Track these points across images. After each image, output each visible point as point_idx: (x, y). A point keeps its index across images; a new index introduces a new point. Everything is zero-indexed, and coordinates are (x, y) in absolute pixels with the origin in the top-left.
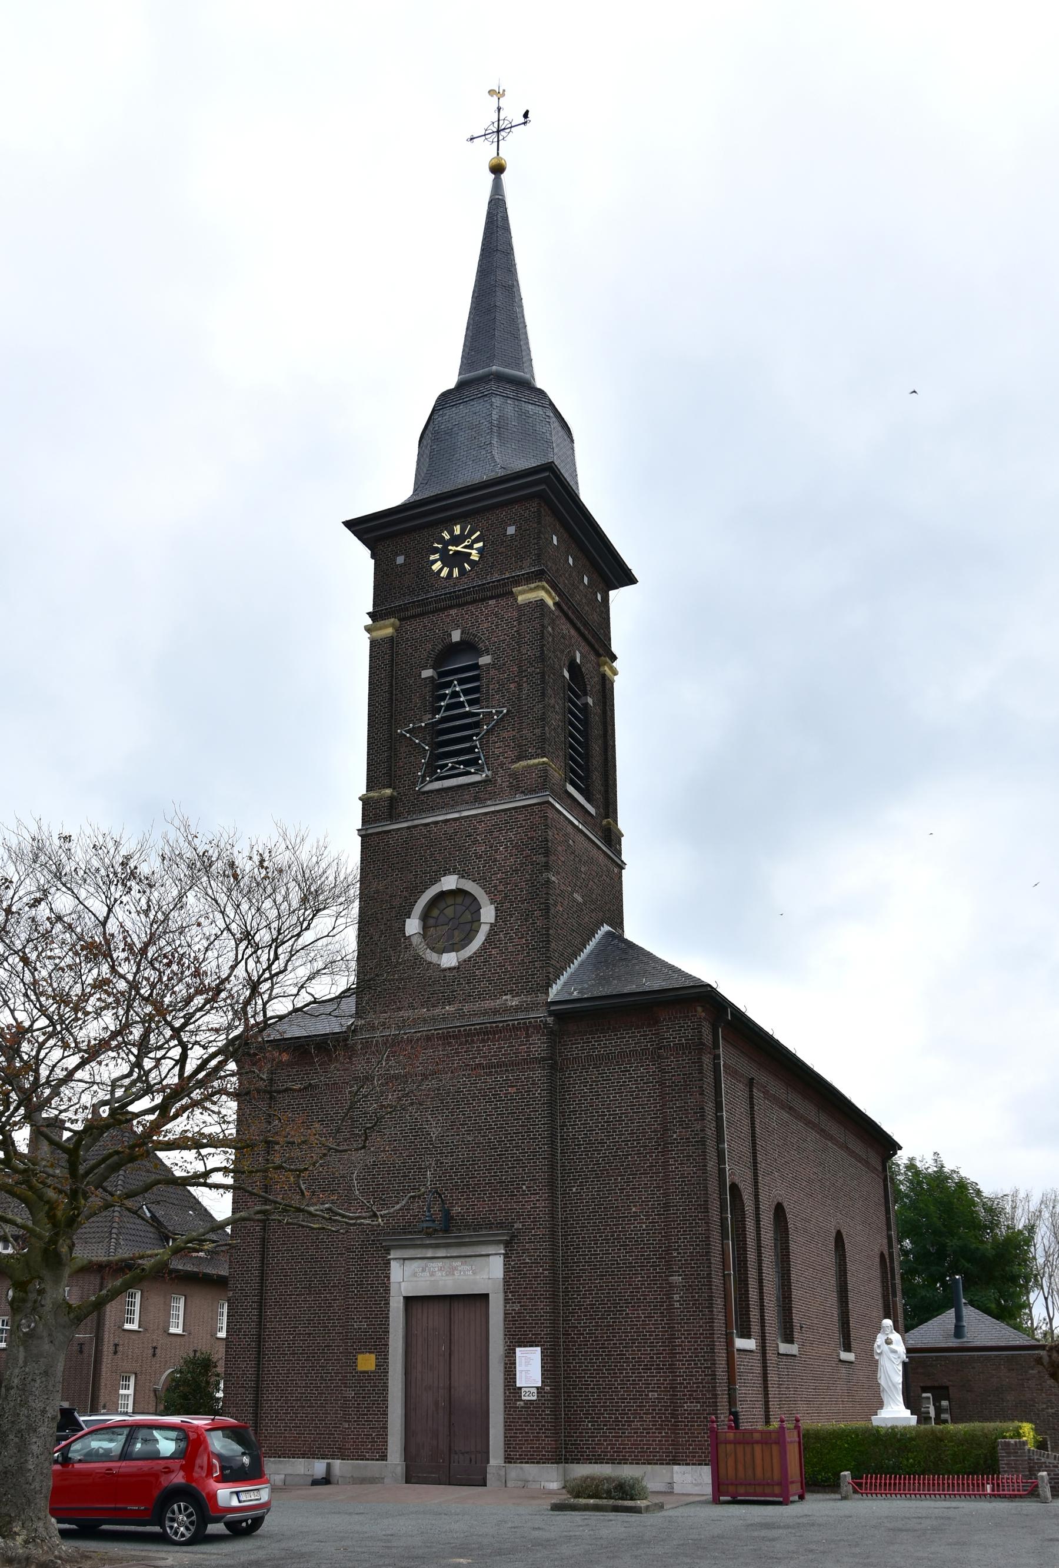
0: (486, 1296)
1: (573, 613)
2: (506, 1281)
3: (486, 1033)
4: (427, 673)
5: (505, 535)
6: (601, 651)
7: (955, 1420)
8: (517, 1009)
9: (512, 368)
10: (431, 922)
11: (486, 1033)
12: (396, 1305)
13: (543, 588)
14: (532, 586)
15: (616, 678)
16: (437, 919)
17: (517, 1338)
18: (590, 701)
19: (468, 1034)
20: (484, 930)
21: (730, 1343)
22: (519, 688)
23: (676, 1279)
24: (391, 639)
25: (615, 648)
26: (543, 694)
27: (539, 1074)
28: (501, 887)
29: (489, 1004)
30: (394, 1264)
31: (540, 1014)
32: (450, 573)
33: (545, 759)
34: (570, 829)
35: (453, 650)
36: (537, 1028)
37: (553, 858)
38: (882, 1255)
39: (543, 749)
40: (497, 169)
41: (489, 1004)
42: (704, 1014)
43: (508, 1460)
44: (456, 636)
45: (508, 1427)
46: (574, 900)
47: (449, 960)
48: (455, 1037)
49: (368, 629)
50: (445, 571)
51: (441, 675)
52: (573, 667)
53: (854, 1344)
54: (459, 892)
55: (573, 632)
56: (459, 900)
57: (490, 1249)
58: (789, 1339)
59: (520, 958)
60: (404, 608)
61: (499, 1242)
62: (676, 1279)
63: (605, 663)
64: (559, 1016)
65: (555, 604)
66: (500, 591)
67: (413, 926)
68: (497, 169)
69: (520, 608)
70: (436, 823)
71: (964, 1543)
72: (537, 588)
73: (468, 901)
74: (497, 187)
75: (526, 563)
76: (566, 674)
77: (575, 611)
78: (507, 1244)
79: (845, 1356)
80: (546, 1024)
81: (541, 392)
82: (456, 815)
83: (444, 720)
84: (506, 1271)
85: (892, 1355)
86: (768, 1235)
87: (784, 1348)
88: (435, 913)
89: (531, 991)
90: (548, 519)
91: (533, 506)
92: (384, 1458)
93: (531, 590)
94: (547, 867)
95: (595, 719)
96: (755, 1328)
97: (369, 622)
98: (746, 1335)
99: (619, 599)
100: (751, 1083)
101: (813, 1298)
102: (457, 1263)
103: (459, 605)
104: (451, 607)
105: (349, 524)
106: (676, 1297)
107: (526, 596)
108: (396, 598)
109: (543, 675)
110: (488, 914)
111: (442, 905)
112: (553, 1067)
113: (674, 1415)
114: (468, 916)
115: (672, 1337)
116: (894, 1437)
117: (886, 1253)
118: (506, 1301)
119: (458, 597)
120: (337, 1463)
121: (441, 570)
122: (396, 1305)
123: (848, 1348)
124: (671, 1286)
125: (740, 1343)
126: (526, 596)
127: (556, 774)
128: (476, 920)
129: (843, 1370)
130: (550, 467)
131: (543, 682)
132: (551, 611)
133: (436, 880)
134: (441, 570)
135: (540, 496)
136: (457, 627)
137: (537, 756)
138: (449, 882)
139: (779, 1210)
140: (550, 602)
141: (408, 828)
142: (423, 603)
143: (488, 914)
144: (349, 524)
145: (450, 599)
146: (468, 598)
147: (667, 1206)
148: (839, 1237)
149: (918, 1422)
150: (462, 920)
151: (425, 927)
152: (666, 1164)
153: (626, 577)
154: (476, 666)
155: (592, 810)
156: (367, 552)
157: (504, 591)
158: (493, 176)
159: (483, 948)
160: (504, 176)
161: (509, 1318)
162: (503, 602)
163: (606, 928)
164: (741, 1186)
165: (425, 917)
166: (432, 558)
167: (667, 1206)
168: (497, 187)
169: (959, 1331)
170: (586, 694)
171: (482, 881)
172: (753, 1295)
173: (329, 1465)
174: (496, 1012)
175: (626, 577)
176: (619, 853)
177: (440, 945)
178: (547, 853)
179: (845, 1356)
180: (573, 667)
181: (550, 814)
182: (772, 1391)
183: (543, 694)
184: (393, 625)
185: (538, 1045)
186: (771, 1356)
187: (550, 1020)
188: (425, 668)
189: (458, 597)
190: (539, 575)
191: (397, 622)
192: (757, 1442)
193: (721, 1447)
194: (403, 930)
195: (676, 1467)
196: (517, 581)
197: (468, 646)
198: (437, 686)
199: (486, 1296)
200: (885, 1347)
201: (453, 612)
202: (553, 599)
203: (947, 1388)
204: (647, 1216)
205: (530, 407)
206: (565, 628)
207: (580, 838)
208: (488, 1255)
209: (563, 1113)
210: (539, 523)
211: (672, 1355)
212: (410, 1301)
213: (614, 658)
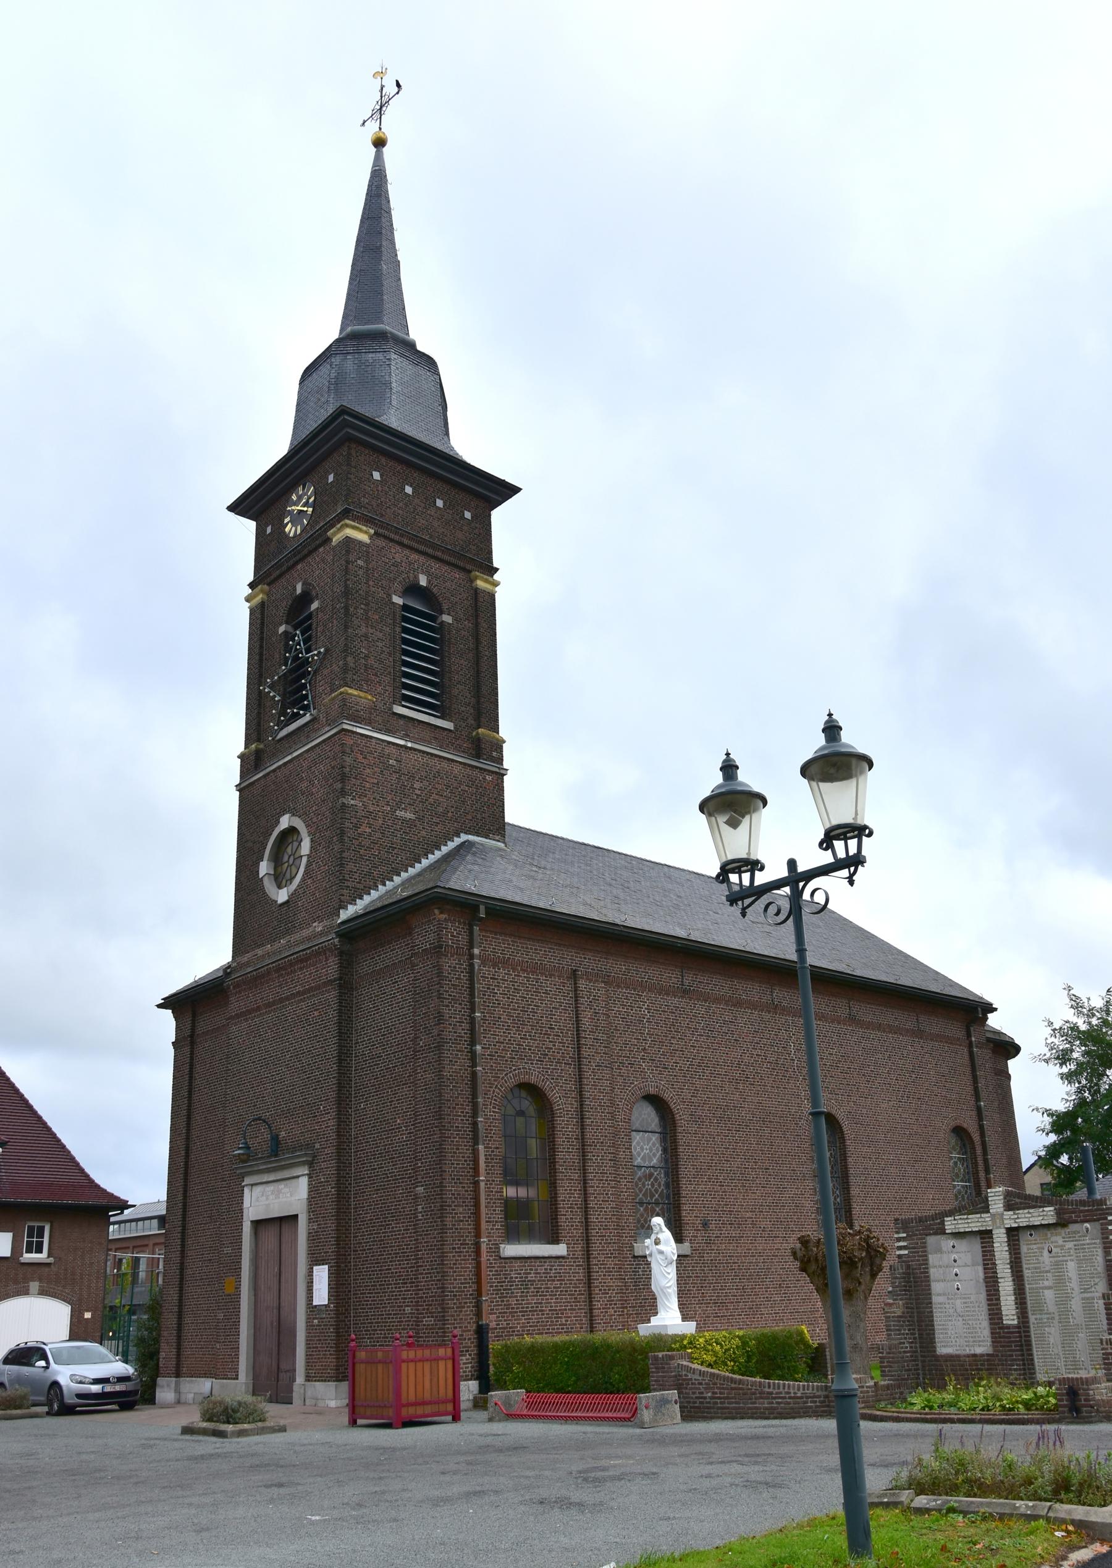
1: (410, 539)
6: (469, 567)
9: (372, 323)
12: (247, 1228)
13: (347, 526)
14: (338, 526)
15: (497, 589)
17: (315, 1260)
19: (291, 965)
28: (315, 820)
30: (246, 1190)
31: (333, 939)
36: (330, 950)
39: (344, 679)
40: (379, 143)
41: (306, 933)
42: (443, 916)
43: (308, 1378)
49: (248, 600)
61: (303, 1163)
68: (379, 143)
72: (340, 530)
74: (379, 160)
78: (310, 1164)
82: (289, 758)
85: (659, 1257)
91: (344, 450)
94: (343, 793)
102: (281, 1186)
104: (297, 563)
105: (514, 490)
122: (247, 1228)
124: (416, 1197)
128: (467, 841)
140: (364, 538)
141: (264, 776)
144: (514, 490)
146: (306, 551)
158: (374, 150)
159: (303, 880)
160: (385, 150)
161: (312, 1237)
168: (379, 160)
170: (442, 613)
174: (309, 939)
181: (349, 741)
184: (262, 591)
190: (346, 514)
191: (266, 587)
192: (380, 1362)
193: (357, 1366)
200: (654, 1248)
202: (366, 532)
205: (371, 355)
208: (298, 1177)
212: (257, 1224)
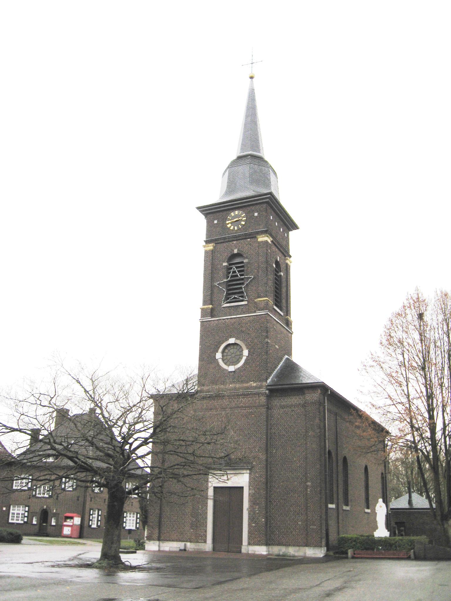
0: (242, 488)
2: (250, 483)
3: (245, 395)
4: (225, 264)
5: (254, 216)
7: (406, 535)
8: (256, 388)
10: (225, 354)
11: (245, 395)
16: (227, 353)
18: (282, 274)
20: (244, 358)
21: (327, 506)
22: (258, 272)
23: (309, 484)
24: (212, 251)
25: (291, 253)
26: (267, 275)
27: (264, 410)
29: (245, 385)
31: (264, 390)
32: (234, 228)
33: (267, 298)
34: (275, 323)
35: (234, 256)
36: (262, 394)
37: (269, 333)
38: (382, 474)
41: (245, 385)
44: (236, 251)
45: (249, 532)
46: (276, 348)
47: (231, 368)
48: (233, 396)
49: (204, 247)
50: (232, 227)
51: (230, 264)
52: (277, 263)
53: (370, 506)
54: (235, 344)
55: (277, 250)
56: (235, 347)
57: (245, 472)
58: (347, 505)
59: (257, 369)
60: (216, 240)
61: (247, 469)
62: (309, 484)
63: (287, 259)
64: (271, 391)
65: (272, 241)
66: (252, 236)
67: (219, 355)
69: (259, 243)
70: (228, 319)
71: (441, 585)
73: (238, 348)
74: (252, 84)
75: (261, 227)
76: (274, 266)
77: (278, 242)
79: (367, 511)
80: (265, 393)
81: (266, 162)
83: (230, 281)
84: (250, 479)
86: (341, 468)
87: (345, 508)
88: (227, 351)
89: (260, 381)
90: (269, 210)
91: (265, 206)
92: (205, 542)
93: (263, 237)
94: (267, 337)
95: (284, 280)
96: (335, 500)
97: (204, 244)
98: (332, 503)
99: (292, 234)
100: (336, 414)
101: (356, 490)
103: (237, 240)
104: (234, 241)
106: (309, 490)
107: (262, 238)
108: (216, 237)
109: (267, 267)
110: (246, 353)
111: (229, 348)
112: (268, 408)
113: (306, 530)
114: (238, 353)
115: (307, 504)
116: (382, 541)
117: (384, 472)
118: (250, 489)
119: (237, 237)
120: (188, 544)
121: (231, 227)
123: (368, 508)
124: (307, 486)
125: (330, 506)
126: (262, 238)
127: (271, 302)
128: (241, 355)
129: (366, 515)
130: (271, 194)
131: (267, 270)
132: (270, 244)
133: (227, 340)
134: (231, 227)
135: (267, 203)
136: (236, 247)
137: (264, 297)
138: (232, 341)
139: (345, 459)
140: (269, 241)
142: (225, 238)
143: (246, 353)
145: (234, 237)
146: (240, 238)
147: (306, 458)
148: (366, 468)
149: (390, 536)
150: (236, 354)
151: (223, 356)
152: (306, 444)
153: (295, 227)
154: (242, 262)
155: (282, 314)
156: (203, 217)
157: (253, 236)
159: (244, 364)
162: (253, 240)
163: (286, 356)
164: (332, 451)
165: (223, 352)
166: (227, 222)
167: (306, 458)
169: (410, 502)
171: (243, 340)
172: (335, 489)
173: (185, 545)
175: (295, 227)
176: (291, 328)
177: (228, 363)
178: (267, 332)
179: (367, 511)
180: (277, 263)
182: (340, 522)
183: (267, 275)
185: (263, 399)
186: (341, 511)
187: (267, 392)
188: (224, 262)
189: (237, 237)
194: (215, 357)
195: (307, 548)
196: (258, 233)
197: (239, 255)
198: (229, 269)
199: (242, 488)
201: (235, 242)
203: (404, 523)
204: (299, 461)
206: (274, 248)
207: (278, 325)
209: (271, 424)
210: (266, 212)
211: (307, 509)
213: (290, 257)
